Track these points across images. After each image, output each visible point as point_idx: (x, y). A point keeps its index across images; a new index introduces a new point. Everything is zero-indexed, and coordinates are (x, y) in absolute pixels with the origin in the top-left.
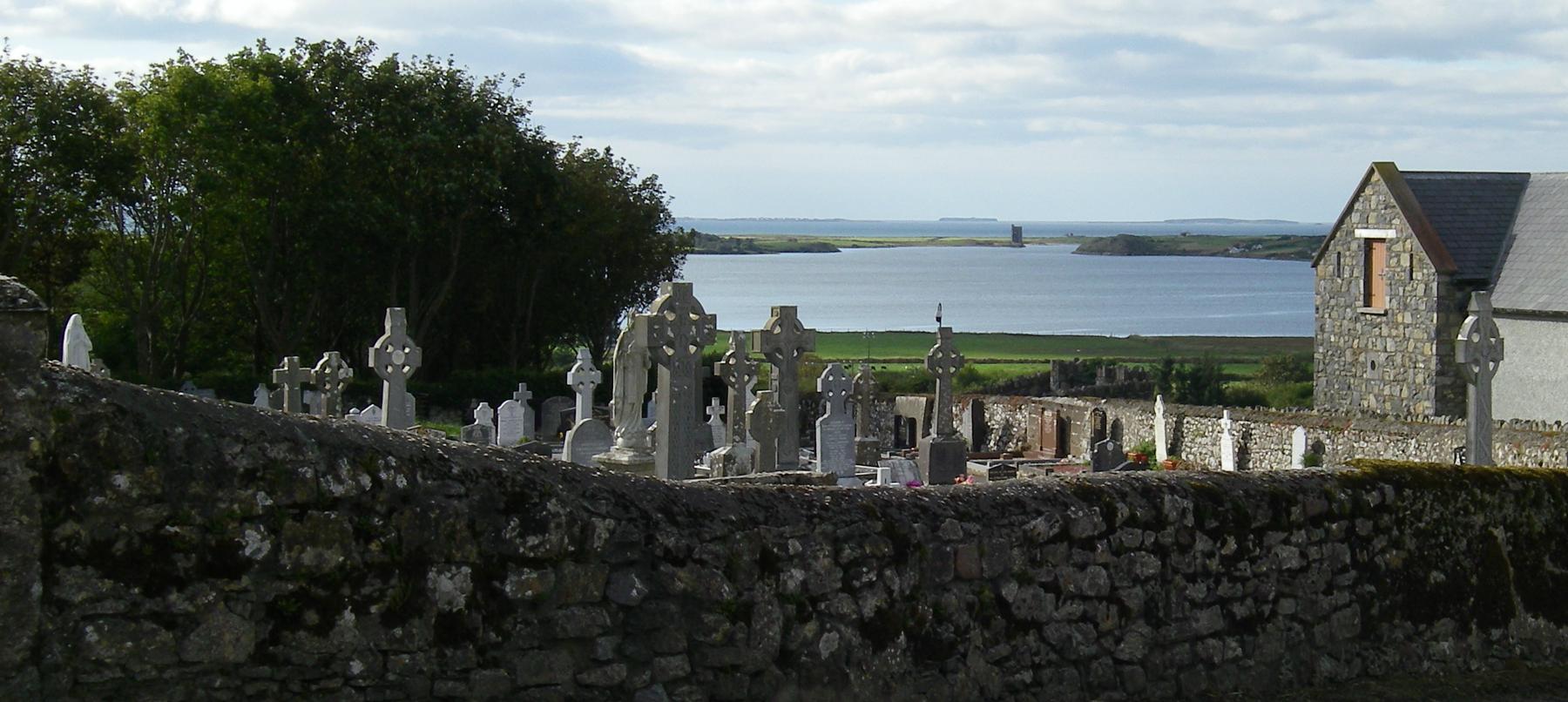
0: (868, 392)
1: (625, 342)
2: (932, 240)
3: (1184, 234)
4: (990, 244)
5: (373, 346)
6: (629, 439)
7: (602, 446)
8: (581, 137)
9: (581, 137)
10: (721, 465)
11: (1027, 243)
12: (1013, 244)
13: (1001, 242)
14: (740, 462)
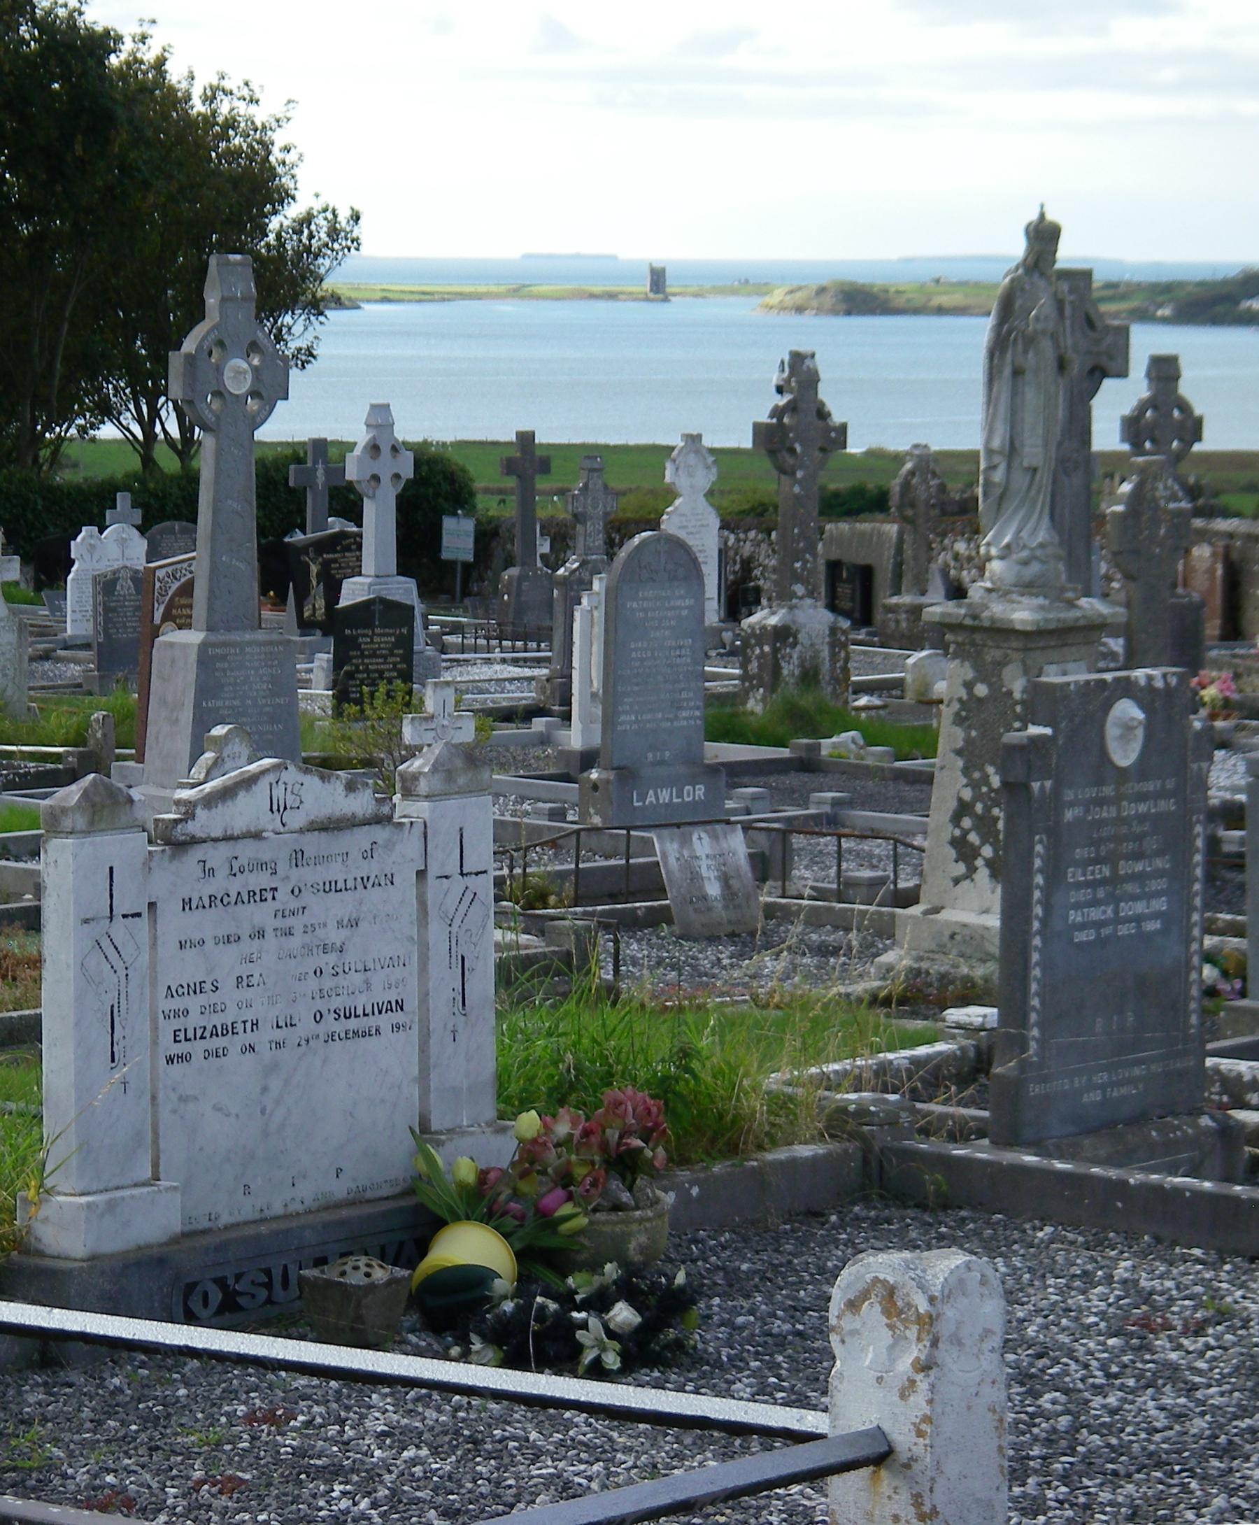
0: (927, 502)
1: (1018, 303)
2: (515, 291)
3: (937, 281)
4: (612, 296)
5: (178, 347)
6: (1025, 563)
7: (681, 597)
8: (154, 22)
9: (154, 22)
10: (767, 649)
11: (675, 295)
12: (651, 295)
13: (630, 293)
14: (807, 642)
